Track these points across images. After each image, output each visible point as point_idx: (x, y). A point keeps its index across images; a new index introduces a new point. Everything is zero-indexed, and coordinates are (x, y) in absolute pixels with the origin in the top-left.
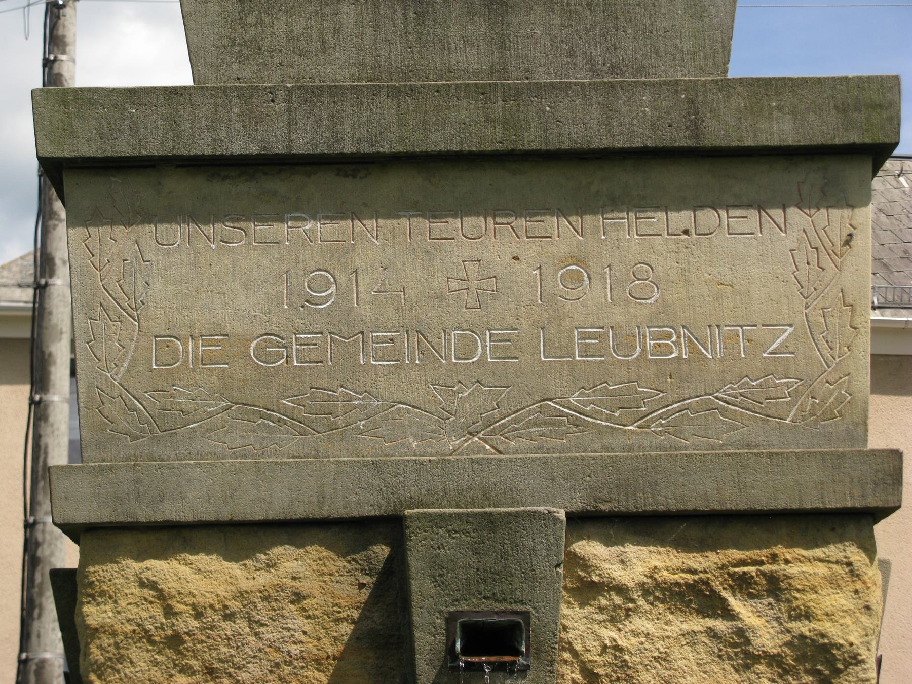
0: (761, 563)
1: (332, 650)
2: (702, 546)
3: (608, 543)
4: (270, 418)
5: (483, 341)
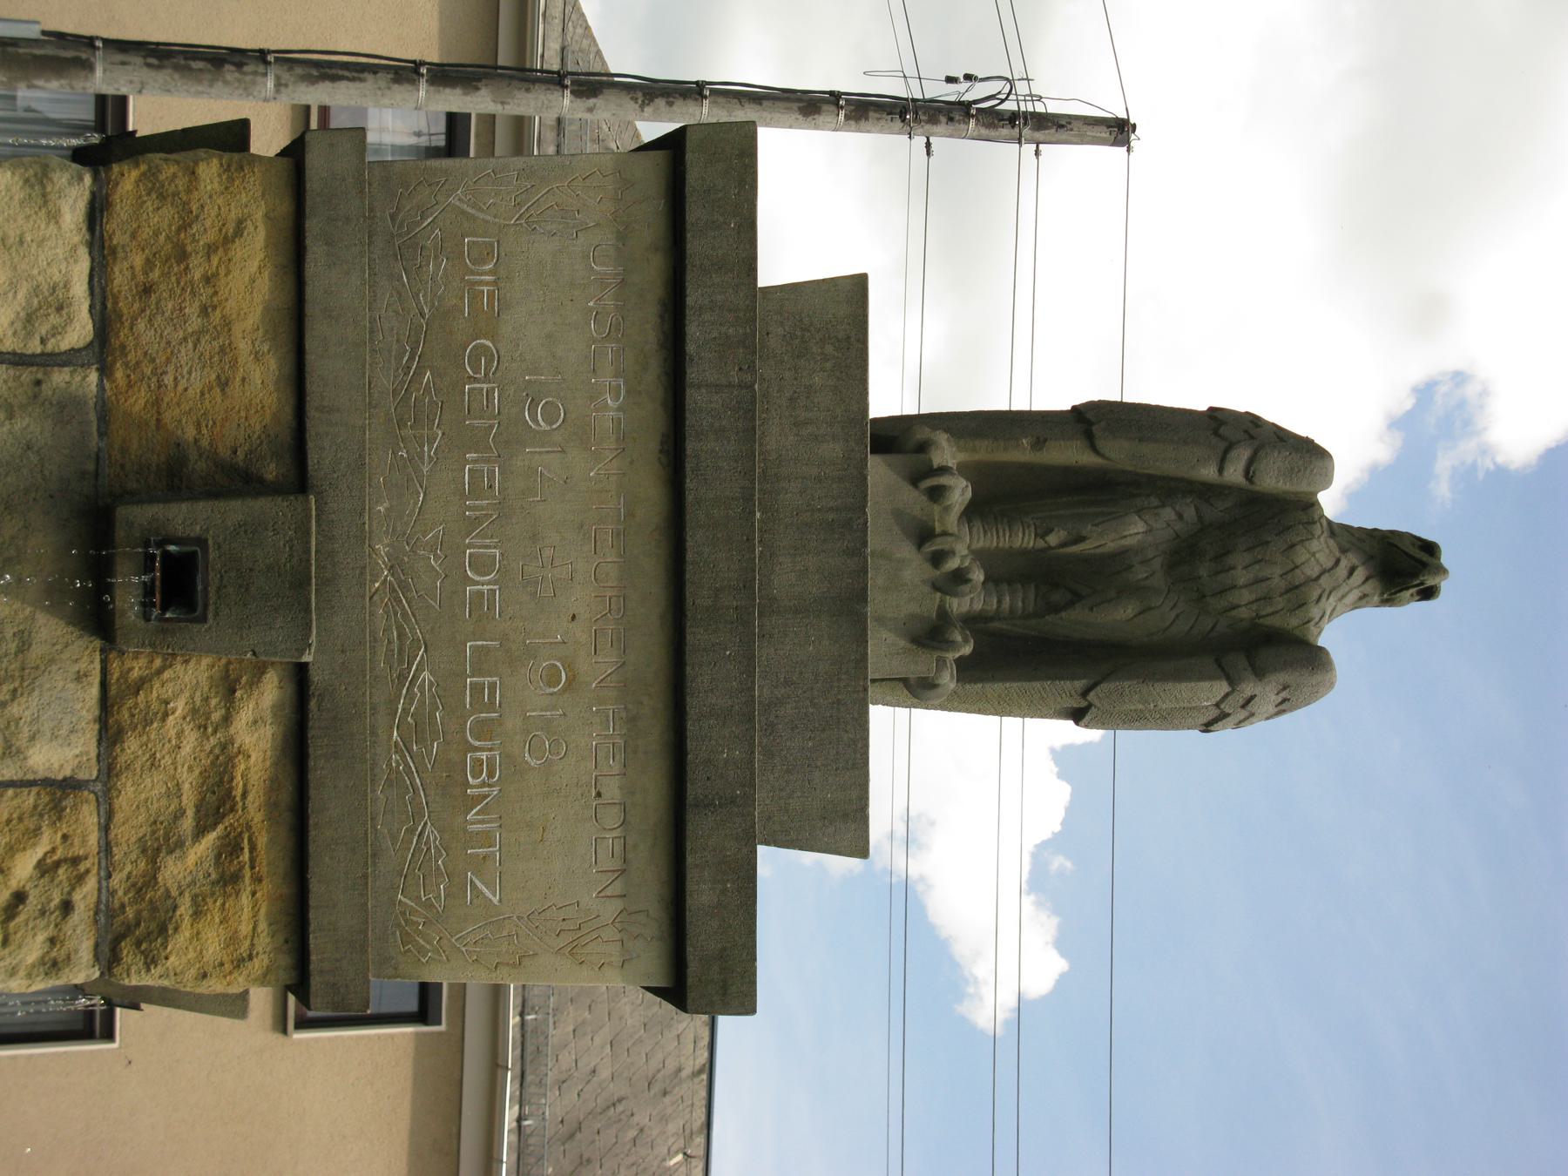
0: (252, 868)
1: (168, 417)
2: (271, 806)
3: (277, 708)
4: (411, 358)
5: (488, 583)
